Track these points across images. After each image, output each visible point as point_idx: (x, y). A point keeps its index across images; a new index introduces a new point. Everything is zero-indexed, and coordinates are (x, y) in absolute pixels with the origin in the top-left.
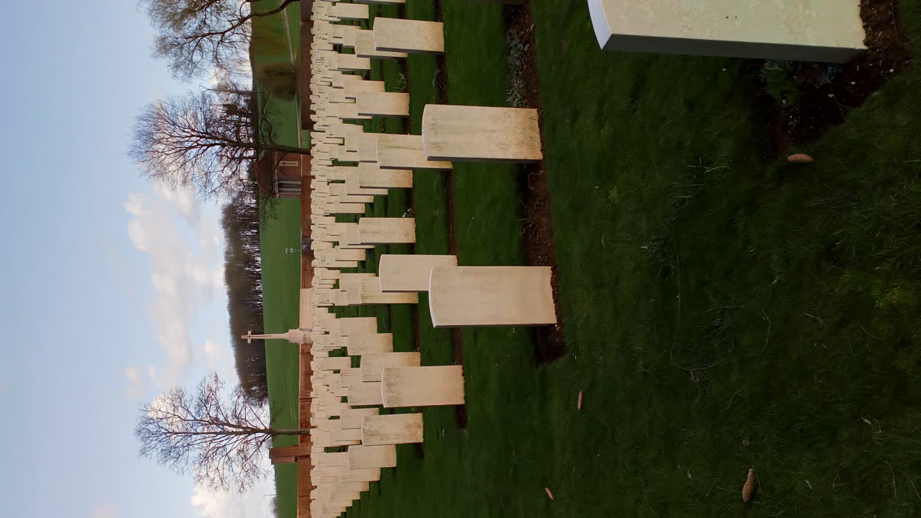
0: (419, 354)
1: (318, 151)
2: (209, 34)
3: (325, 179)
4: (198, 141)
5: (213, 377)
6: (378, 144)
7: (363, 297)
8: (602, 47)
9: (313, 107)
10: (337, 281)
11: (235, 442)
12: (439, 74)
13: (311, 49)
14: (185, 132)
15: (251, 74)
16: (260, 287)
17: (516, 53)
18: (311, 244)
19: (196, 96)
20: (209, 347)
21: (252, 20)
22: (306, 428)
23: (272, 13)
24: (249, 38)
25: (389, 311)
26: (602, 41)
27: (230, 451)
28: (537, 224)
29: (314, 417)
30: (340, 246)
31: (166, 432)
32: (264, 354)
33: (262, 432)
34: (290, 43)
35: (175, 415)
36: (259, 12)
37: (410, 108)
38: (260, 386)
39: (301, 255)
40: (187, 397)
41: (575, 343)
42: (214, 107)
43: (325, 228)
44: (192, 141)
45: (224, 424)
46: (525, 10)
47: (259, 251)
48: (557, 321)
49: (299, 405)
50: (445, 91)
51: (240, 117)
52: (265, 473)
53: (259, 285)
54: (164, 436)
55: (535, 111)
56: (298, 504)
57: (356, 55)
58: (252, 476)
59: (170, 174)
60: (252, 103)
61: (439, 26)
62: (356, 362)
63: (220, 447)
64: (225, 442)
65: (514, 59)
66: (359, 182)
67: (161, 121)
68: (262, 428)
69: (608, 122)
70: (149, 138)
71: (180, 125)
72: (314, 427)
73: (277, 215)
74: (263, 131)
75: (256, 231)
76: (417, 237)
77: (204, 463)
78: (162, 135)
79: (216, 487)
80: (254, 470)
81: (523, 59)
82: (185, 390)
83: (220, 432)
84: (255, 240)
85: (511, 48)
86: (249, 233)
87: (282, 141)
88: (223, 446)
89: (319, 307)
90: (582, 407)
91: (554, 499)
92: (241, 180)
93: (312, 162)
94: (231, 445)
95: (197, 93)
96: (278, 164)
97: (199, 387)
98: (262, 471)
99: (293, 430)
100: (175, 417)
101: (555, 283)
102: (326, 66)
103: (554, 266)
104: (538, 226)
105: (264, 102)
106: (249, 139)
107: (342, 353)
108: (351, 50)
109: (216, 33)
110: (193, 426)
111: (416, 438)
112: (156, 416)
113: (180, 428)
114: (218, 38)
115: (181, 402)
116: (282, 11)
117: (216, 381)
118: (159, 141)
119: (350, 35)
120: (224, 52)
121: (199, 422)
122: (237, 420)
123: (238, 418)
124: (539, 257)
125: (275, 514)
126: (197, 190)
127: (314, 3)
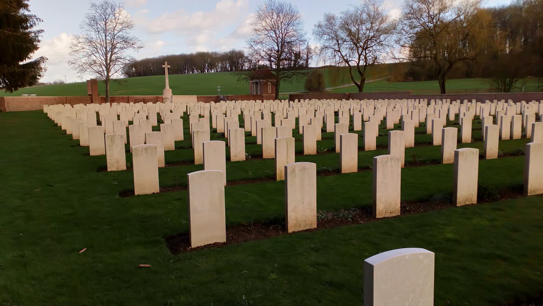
0: (164, 166)
1: (278, 104)
2: (338, 43)
3: (263, 108)
4: (280, 38)
5: (141, 45)
6: (289, 138)
7: (197, 132)
8: (365, 260)
9: (302, 100)
10: (203, 117)
11: (101, 59)
12: (329, 171)
13: (334, 99)
14: (284, 30)
15: (319, 66)
16: (196, 72)
17: (347, 214)
18: (224, 101)
19: (304, 36)
20: (160, 43)
21: (348, 67)
22: (110, 100)
23: (352, 77)
24: (337, 65)
25: (189, 148)
26: (369, 260)
27: (95, 56)
28: (251, 232)
29: (118, 105)
30: (225, 118)
31: (107, 18)
32: (155, 75)
34: (337, 87)
35: (117, 23)
36: (352, 71)
37: (309, 155)
40: (128, 30)
41: (181, 260)
43: (234, 109)
44: (279, 34)
45: (112, 52)
47: (217, 71)
48: (193, 248)
51: (294, 61)
52: (81, 76)
54: (104, 17)
55: (316, 226)
56: (61, 97)
57: (507, 106)
58: (79, 69)
59: (260, 22)
60: (301, 67)
61: (355, 170)
62: (156, 129)
63: (97, 50)
64: (101, 53)
65: (343, 213)
67: (290, 18)
68: (110, 74)
69: (314, 269)
70: (279, 11)
71: (288, 27)
72: (111, 105)
74: (287, 73)
75: (229, 69)
76: (234, 162)
77: (87, 40)
79: (72, 48)
80: (83, 70)
81: (344, 218)
82: (133, 30)
83: (107, 50)
84: (224, 69)
86: (228, 66)
87: (282, 84)
88: (98, 52)
89: (187, 106)
91: (79, 254)
92: (258, 61)
93: (271, 101)
94: (99, 56)
95: (306, 37)
96: (269, 82)
97: (135, 37)
98: (82, 75)
100: (116, 23)
101: (216, 244)
102: (326, 108)
104: (249, 233)
105: (304, 74)
106: (282, 65)
108: (337, 121)
109: (339, 48)
112: (116, 13)
113: (109, 26)
114: (336, 48)
115: (125, 27)
116: (353, 83)
117: (139, 47)
118: (278, 16)
119: (344, 120)
120: (330, 52)
122: (114, 59)
123: (116, 60)
124: (231, 235)
126: (252, 37)
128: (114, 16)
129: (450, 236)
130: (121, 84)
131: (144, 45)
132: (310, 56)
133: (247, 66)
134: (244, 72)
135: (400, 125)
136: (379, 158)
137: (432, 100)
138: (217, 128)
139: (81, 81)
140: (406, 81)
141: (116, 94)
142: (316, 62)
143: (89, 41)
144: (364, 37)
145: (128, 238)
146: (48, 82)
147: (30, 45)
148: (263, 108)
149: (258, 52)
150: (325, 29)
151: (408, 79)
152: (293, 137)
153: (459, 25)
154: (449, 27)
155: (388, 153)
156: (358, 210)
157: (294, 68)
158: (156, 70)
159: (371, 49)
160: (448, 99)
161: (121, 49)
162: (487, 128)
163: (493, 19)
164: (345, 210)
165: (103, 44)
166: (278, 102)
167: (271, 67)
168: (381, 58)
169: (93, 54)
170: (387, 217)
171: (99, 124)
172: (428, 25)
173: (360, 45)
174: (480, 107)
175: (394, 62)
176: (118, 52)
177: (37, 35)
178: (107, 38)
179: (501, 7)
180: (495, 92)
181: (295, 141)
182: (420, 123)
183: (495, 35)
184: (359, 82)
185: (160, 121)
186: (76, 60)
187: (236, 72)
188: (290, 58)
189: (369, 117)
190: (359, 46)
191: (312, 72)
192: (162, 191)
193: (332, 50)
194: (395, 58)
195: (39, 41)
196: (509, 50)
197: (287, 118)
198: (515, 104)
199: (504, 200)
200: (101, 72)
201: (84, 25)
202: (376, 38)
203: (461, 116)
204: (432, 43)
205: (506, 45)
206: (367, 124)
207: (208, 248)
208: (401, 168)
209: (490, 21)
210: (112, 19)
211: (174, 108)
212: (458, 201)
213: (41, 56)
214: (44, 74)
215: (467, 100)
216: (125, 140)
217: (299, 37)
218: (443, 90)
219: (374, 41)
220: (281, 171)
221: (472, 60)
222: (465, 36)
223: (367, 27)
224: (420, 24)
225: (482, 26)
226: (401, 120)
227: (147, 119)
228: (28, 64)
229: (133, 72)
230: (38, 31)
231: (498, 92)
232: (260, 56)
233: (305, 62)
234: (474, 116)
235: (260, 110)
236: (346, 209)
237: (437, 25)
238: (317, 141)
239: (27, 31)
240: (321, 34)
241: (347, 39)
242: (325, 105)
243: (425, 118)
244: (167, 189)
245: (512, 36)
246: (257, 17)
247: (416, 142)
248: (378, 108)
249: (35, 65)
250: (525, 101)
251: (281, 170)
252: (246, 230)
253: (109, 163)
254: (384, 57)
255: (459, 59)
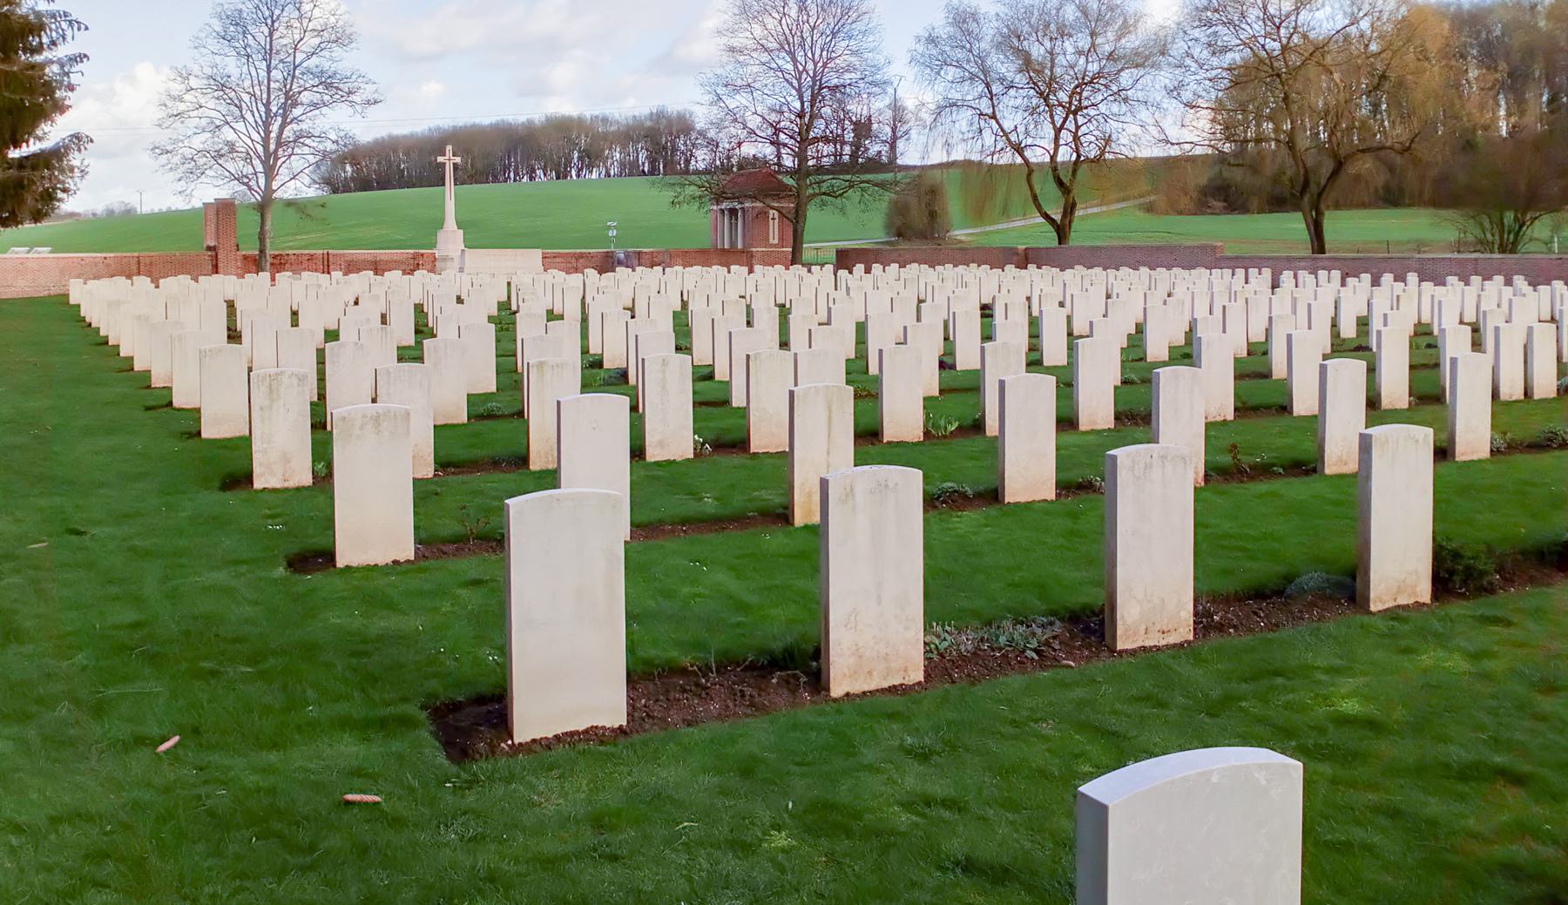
0: (431, 475)
2: (990, 92)
3: (751, 290)
4: (807, 73)
5: (376, 96)
7: (541, 365)
9: (877, 268)
10: (561, 317)
11: (250, 137)
12: (964, 496)
13: (979, 266)
16: (542, 177)
17: (1021, 635)
18: (627, 267)
19: (885, 70)
20: (432, 88)
21: (1020, 165)
22: (272, 264)
23: (1035, 198)
24: (989, 160)
25: (512, 415)
26: (1090, 789)
28: (707, 694)
30: (630, 321)
31: (275, 17)
32: (414, 186)
33: (266, 184)
34: (988, 229)
35: (305, 32)
36: (1035, 178)
38: (352, 178)
39: (605, 250)
40: (338, 51)
41: (478, 782)
42: (865, 101)
43: (659, 292)
44: (806, 63)
45: (285, 117)
46: (1096, 649)
47: (609, 176)
48: (520, 744)
49: (315, 251)
50: (936, 507)
52: (188, 192)
53: (545, 175)
56: (125, 254)
58: (183, 168)
60: (875, 165)
62: (411, 355)
63: (241, 112)
64: (251, 119)
66: (757, 354)
68: (275, 185)
71: (833, 43)
72: (273, 279)
73: (678, 206)
74: (829, 182)
75: (646, 169)
77: (212, 82)
78: (813, 12)
79: (165, 105)
80: (194, 171)
81: (1010, 649)
82: (352, 49)
85: (1028, 626)
87: (815, 217)
88: (242, 117)
89: (509, 284)
90: (348, 803)
91: (157, 754)
92: (739, 145)
93: (779, 268)
95: (890, 72)
96: (773, 208)
97: (358, 73)
98: (192, 186)
99: (268, 240)
100: (302, 32)
101: (593, 734)
103: (628, 730)
104: (704, 695)
105: (882, 185)
106: (813, 158)
107: (421, 328)
108: (987, 337)
109: (993, 107)
110: (283, 63)
111: (262, 475)
114: (985, 106)
117: (368, 102)
119: (1012, 333)
120: (964, 118)
121: (291, 73)
122: (291, 139)
123: (295, 141)
124: (643, 701)
125: (105, 212)
126: (719, 72)
127: (1058, 269)
128: (299, 9)
129: (1351, 706)
130: (308, 215)
131: (382, 95)
132: (901, 130)
133: (704, 159)
134: (693, 177)
135: (1187, 351)
136: (1126, 456)
137: (1285, 272)
138: (602, 354)
139: (188, 207)
140: (1203, 213)
141: (291, 244)
142: (920, 148)
143: (217, 85)
144: (1069, 75)
145: (311, 708)
146: (87, 211)
147: (45, 100)
148: (751, 290)
149: (738, 116)
150: (948, 49)
151: (1209, 207)
152: (847, 383)
153: (1356, 48)
154: (1328, 52)
155: (1154, 439)
156: (1058, 622)
157: (853, 167)
158: (416, 172)
159: (1092, 112)
160: (1333, 271)
161: (312, 108)
162: (1454, 361)
163: (1456, 32)
164: (1017, 622)
165: (259, 93)
166: (801, 272)
167: (779, 164)
168: (1123, 141)
169: (228, 123)
170: (1151, 647)
171: (234, 338)
172: (1263, 46)
173: (1058, 101)
174: (1433, 296)
175: (1165, 155)
176: (304, 116)
177: (66, 70)
178: (272, 74)
179: (446, 128)
180: (1474, 251)
181: (855, 398)
182: (1249, 344)
183: (1464, 82)
184: (1057, 213)
185: (425, 329)
186: (175, 142)
187: (669, 179)
188: (838, 136)
189: (1091, 323)
190: (1056, 103)
191: (908, 180)
192: (424, 556)
193: (970, 112)
194: (1167, 142)
195: (71, 88)
196: (1508, 124)
197: (829, 323)
198: (1535, 291)
199: (1512, 589)
200: (248, 178)
201: (207, 37)
202: (1106, 78)
203: (1376, 324)
204: (1278, 97)
205: (1498, 111)
206: (1083, 345)
207: (567, 746)
208: (1195, 488)
209: (1447, 38)
210: (290, 19)
211: (470, 288)
212: (1372, 595)
213: (73, 133)
214: (78, 185)
215: (1392, 275)
216: (312, 390)
217: (867, 73)
218: (1318, 244)
219: (1102, 87)
220: (810, 495)
221: (1399, 153)
222: (1376, 80)
223: (1080, 44)
224: (1240, 42)
225: (1424, 53)
226: (1190, 334)
227: (382, 323)
228: (35, 155)
229: (346, 178)
230: (71, 59)
231: (1482, 253)
232: (744, 128)
233: (885, 149)
234: (1415, 325)
235: (741, 297)
236: (1021, 618)
237: (1292, 44)
238: (925, 399)
239: (38, 58)
240: (937, 65)
241: (1017, 80)
242: (950, 285)
243: (1267, 330)
244: (438, 549)
245: (1515, 84)
246: (736, 11)
247: (1239, 405)
248: (1118, 294)
249: (51, 160)
250: (1562, 282)
251: (807, 490)
252: (693, 688)
253: (261, 464)
254: (1133, 138)
255: (1361, 148)
